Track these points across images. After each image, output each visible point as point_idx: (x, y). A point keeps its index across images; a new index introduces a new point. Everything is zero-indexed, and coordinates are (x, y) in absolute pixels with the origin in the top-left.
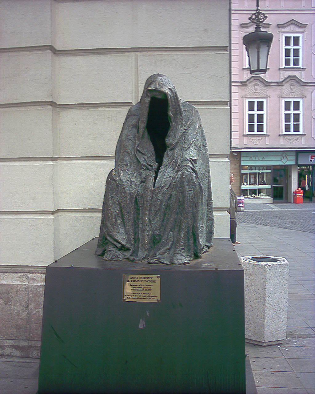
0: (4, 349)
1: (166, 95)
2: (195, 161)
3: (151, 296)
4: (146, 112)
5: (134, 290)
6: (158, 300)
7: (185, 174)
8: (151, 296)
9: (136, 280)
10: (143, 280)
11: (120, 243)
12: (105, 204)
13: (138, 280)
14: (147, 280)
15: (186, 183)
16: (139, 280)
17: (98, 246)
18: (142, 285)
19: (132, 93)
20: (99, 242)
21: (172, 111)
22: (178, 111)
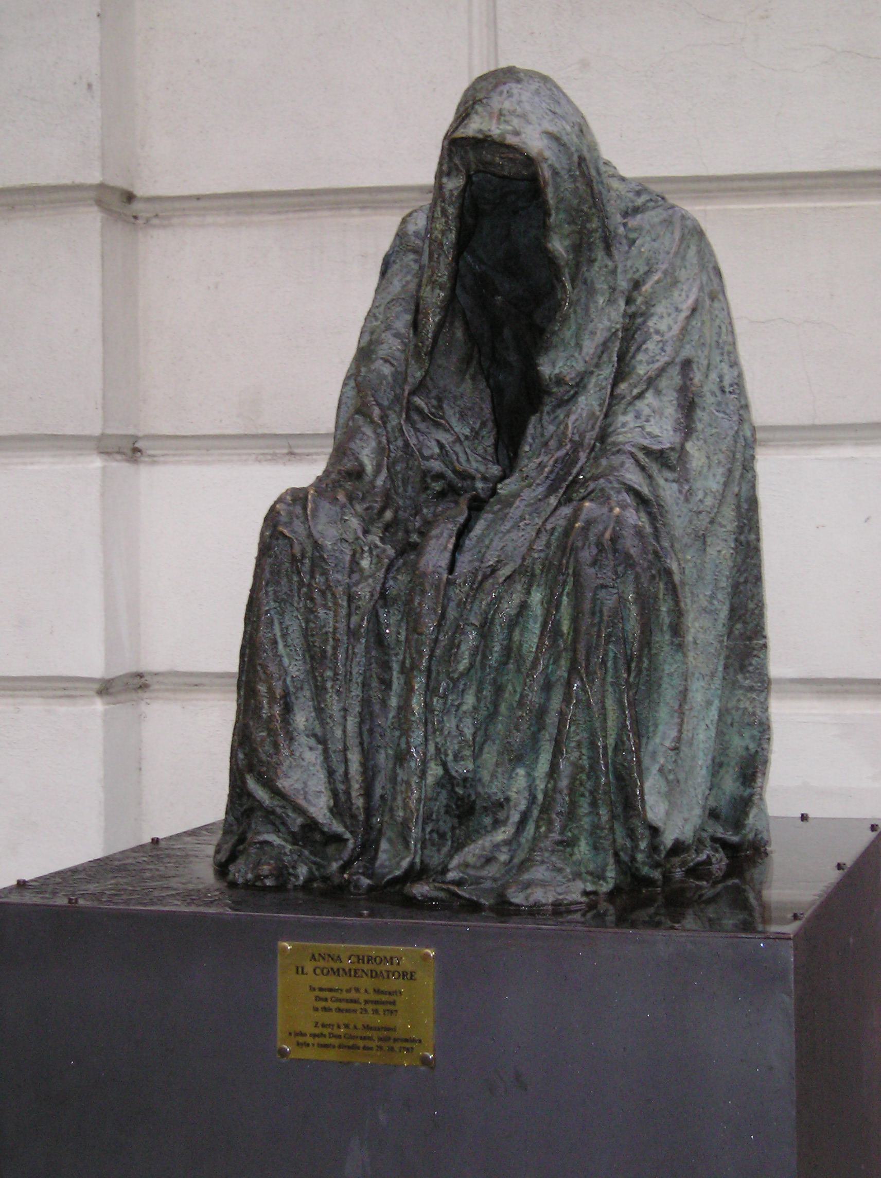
1: (530, 161)
3: (396, 1040)
5: (325, 1009)
7: (583, 516)
8: (396, 1040)
10: (361, 966)
12: (251, 650)
15: (586, 555)
18: (357, 990)
21: (563, 237)
22: (598, 235)
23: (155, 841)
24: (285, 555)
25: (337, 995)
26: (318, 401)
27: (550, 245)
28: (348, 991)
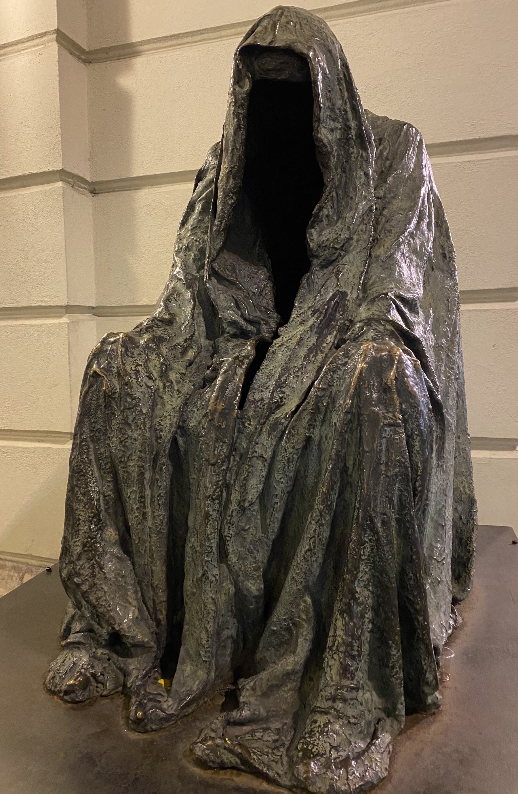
27: (319, 136)
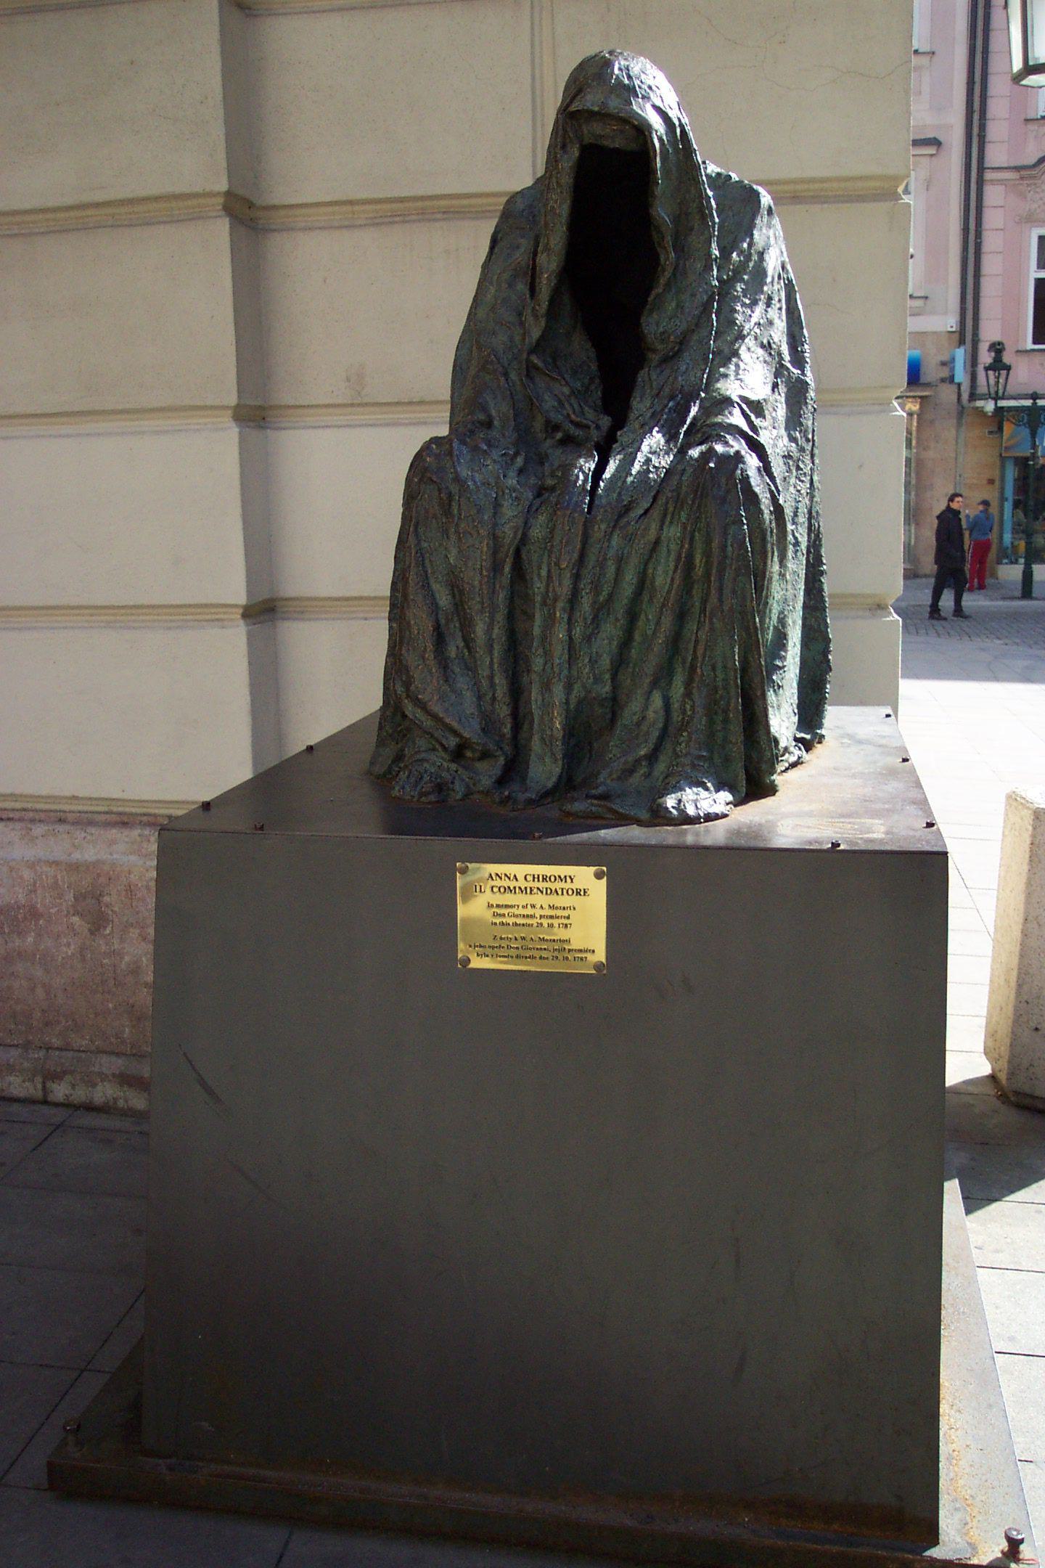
0: (94, 1085)
1: (642, 130)
2: (757, 408)
4: (561, 206)
6: (598, 966)
9: (512, 884)
11: (456, 733)
13: (517, 884)
14: (553, 886)
16: (522, 884)
17: (381, 742)
18: (533, 906)
19: (510, 153)
20: (381, 728)
23: (310, 748)
24: (428, 479)
25: (515, 911)
26: (434, 372)
28: (525, 907)
